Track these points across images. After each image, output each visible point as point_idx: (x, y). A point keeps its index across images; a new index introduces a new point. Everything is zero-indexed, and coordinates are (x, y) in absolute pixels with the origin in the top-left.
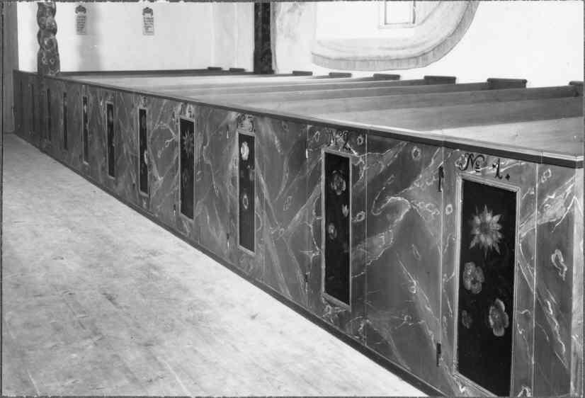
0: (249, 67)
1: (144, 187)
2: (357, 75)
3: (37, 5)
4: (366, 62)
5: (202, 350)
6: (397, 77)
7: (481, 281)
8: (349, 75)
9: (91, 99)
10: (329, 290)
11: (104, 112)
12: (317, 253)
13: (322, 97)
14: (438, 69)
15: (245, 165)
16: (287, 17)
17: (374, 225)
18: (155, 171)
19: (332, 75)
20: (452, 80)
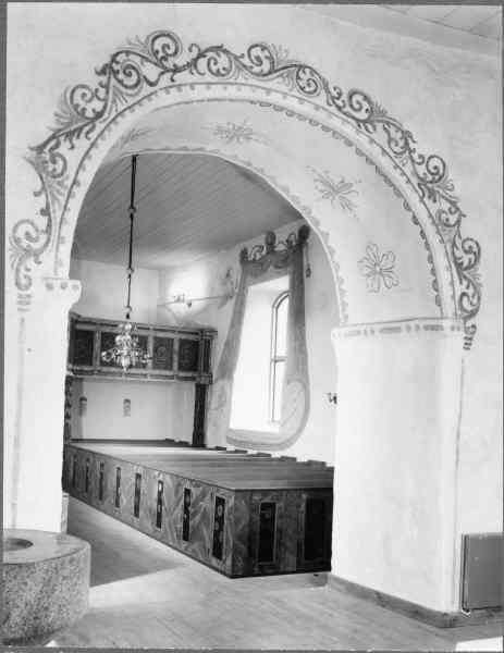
0: (190, 440)
1: (117, 505)
2: (250, 452)
3: (96, 588)
4: (254, 445)
5: (201, 639)
6: (269, 455)
7: (287, 555)
8: (246, 452)
9: (91, 460)
10: (214, 554)
11: (98, 466)
12: (180, 526)
13: (234, 465)
14: (288, 453)
15: (160, 493)
16: (214, 412)
17: (195, 513)
18: (122, 497)
19: (236, 451)
20: (294, 459)
